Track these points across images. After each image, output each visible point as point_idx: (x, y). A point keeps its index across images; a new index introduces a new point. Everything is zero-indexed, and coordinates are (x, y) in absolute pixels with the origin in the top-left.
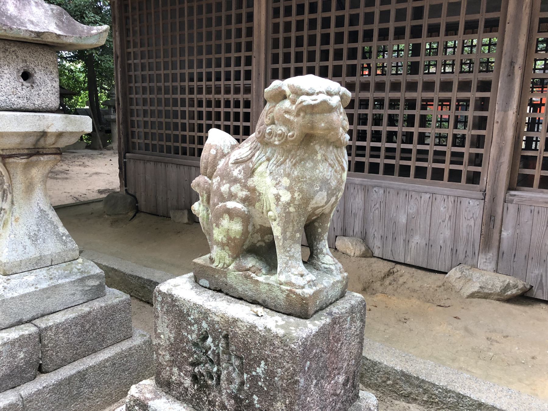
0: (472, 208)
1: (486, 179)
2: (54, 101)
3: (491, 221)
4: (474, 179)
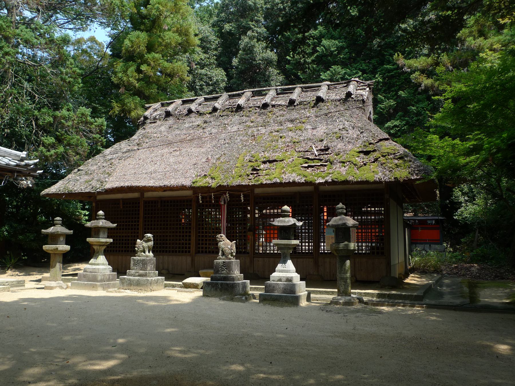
0: (189, 259)
1: (191, 252)
2: (106, 237)
3: (193, 260)
4: (189, 252)
